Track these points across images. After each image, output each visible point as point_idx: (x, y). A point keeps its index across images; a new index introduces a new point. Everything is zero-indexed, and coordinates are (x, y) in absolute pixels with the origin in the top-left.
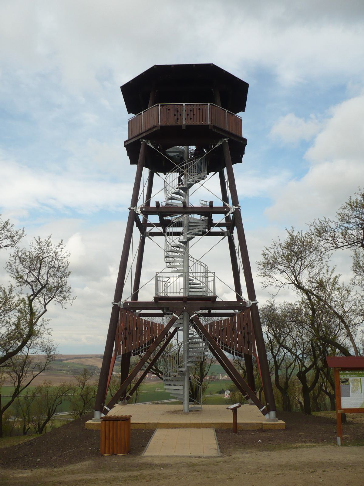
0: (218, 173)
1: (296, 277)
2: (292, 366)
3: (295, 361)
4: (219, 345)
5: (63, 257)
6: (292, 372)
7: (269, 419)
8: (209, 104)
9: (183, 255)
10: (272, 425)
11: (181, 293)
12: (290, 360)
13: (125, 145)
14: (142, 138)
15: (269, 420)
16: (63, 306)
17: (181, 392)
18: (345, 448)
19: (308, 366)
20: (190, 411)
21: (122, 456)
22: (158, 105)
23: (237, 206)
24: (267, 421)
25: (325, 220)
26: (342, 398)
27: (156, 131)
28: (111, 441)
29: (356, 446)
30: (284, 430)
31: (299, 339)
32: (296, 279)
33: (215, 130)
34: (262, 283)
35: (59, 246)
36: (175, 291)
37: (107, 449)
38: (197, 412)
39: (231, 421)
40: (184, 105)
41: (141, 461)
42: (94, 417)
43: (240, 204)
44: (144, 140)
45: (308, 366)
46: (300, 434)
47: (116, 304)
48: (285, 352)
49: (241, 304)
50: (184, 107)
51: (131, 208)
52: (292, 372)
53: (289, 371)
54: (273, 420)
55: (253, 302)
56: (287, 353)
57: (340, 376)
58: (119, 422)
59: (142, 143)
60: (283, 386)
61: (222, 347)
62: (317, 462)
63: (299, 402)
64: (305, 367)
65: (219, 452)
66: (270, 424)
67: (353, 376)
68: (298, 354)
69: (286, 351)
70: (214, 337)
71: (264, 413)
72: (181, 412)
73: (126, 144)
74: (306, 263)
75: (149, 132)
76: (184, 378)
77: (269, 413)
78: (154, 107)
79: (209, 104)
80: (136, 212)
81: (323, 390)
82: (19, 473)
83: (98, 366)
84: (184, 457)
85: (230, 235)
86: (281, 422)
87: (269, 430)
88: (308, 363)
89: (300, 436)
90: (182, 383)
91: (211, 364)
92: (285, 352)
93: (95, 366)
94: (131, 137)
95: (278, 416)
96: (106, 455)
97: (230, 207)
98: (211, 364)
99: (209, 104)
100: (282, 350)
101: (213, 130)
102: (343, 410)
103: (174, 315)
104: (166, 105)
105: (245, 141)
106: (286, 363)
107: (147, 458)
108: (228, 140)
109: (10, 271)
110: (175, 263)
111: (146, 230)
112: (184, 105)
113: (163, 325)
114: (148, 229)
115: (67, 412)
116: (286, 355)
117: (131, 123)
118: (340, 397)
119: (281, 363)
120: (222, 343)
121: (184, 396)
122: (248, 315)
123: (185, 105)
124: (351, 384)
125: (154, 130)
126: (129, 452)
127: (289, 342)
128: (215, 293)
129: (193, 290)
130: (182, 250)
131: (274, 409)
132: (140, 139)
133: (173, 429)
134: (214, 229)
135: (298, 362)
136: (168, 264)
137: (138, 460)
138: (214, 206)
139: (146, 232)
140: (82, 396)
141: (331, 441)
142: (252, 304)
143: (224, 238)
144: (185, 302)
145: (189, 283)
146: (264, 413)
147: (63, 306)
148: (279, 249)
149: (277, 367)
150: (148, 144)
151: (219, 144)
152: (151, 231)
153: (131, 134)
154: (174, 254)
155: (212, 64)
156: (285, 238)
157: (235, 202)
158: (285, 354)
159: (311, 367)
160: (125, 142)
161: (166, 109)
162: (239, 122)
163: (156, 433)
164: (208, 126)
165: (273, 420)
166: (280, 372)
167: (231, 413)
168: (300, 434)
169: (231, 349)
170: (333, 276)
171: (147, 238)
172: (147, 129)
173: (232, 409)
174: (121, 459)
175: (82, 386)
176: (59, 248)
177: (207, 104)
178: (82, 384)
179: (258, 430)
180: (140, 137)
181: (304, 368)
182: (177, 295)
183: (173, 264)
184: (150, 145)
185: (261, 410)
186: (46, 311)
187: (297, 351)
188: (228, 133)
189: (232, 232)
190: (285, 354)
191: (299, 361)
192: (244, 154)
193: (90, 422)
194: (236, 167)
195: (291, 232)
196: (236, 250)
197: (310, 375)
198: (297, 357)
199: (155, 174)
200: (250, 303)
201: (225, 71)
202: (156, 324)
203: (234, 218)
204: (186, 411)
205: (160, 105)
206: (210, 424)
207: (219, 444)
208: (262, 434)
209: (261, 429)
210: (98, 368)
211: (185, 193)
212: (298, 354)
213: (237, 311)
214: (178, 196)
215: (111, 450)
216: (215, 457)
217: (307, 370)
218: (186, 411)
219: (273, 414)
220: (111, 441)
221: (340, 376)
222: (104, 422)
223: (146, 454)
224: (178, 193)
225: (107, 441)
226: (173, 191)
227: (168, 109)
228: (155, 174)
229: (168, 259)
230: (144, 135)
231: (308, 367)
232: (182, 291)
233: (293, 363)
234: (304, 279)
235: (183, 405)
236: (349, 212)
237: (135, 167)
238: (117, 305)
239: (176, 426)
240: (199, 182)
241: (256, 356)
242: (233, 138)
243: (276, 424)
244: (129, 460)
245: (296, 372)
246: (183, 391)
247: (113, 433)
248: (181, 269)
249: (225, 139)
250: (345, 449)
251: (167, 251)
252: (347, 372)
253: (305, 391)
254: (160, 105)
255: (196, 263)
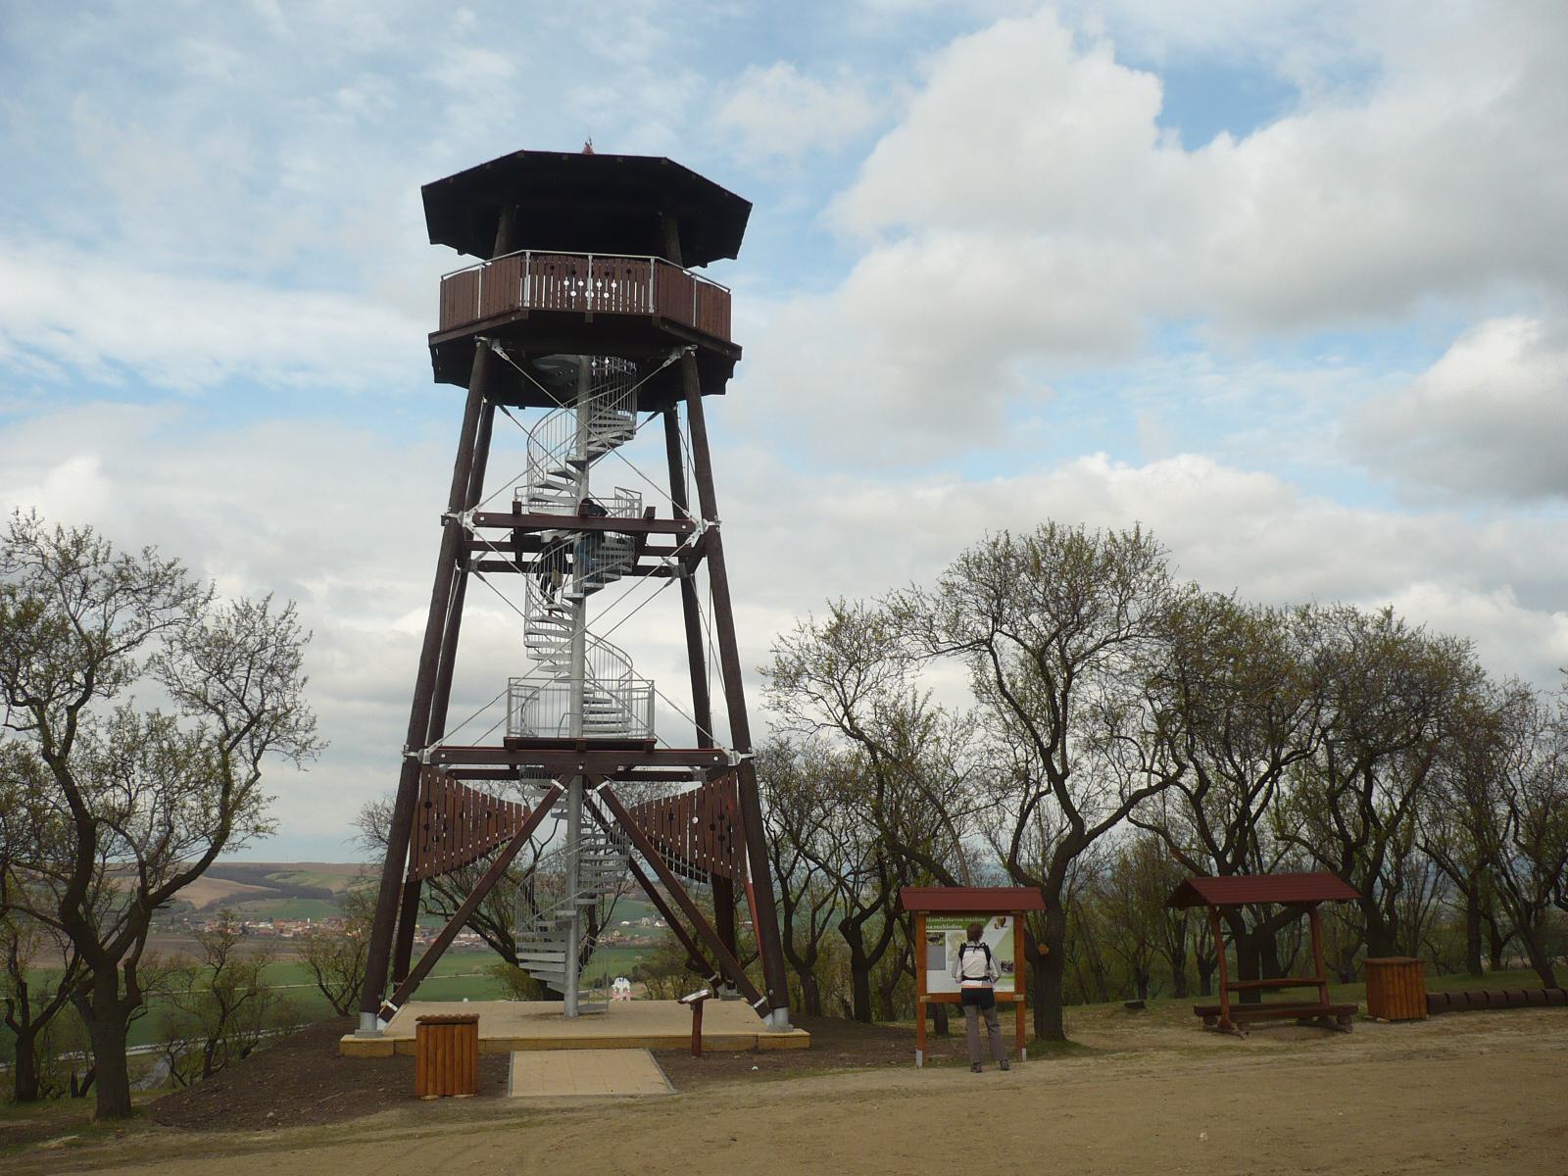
0: (661, 415)
1: (846, 708)
2: (828, 906)
3: (835, 890)
4: (664, 859)
5: (293, 642)
6: (826, 921)
7: (776, 1025)
8: (652, 261)
9: (570, 629)
10: (779, 1040)
11: (564, 729)
12: (823, 888)
13: (433, 343)
14: (480, 334)
15: (771, 1028)
16: (299, 765)
17: (560, 968)
18: (930, 1070)
19: (867, 906)
20: (580, 1014)
21: (466, 1098)
22: (525, 253)
23: (713, 520)
24: (767, 1031)
25: (912, 589)
26: (928, 972)
27: (519, 321)
28: (439, 1068)
29: (617, 573)
30: (805, 1049)
31: (849, 834)
32: (847, 713)
33: (667, 327)
34: (771, 724)
35: (284, 618)
36: (549, 725)
37: (430, 1085)
38: (598, 1016)
39: (688, 1031)
40: (590, 258)
41: (510, 1106)
42: (359, 1028)
43: (721, 515)
44: (483, 338)
45: (867, 906)
46: (842, 1055)
47: (412, 754)
48: (812, 868)
49: (716, 758)
50: (590, 264)
51: (451, 515)
52: (826, 921)
53: (821, 916)
54: (783, 1029)
55: (744, 756)
56: (815, 869)
57: (927, 927)
58: (458, 1027)
59: (478, 344)
60: (803, 957)
61: (671, 863)
62: (871, 1091)
63: (844, 1001)
64: (860, 906)
65: (671, 1087)
66: (775, 1037)
67: (953, 927)
68: (843, 873)
69: (812, 865)
70: (650, 838)
71: (763, 1012)
72: (558, 1017)
73: (436, 340)
74: (869, 681)
75: (500, 322)
76: (568, 934)
77: (773, 1014)
78: (514, 258)
79: (652, 261)
80: (460, 526)
81: (906, 968)
82: (249, 1136)
83: (193, 901)
84: (599, 1096)
85: (686, 576)
86: (800, 1032)
87: (773, 1051)
88: (868, 894)
89: (841, 1059)
90: (561, 946)
91: (616, 899)
92: (812, 868)
93: (183, 900)
94: (447, 327)
95: (794, 1021)
96: (428, 1097)
97: (695, 522)
98: (616, 899)
99: (653, 259)
100: (803, 864)
101: (661, 328)
102: (930, 997)
103: (555, 782)
104: (545, 254)
105: (736, 352)
106: (813, 896)
107: (522, 1101)
108: (696, 351)
109: (162, 677)
110: (548, 652)
111: (469, 555)
112: (590, 258)
113: (527, 808)
114: (475, 555)
115: (143, 1047)
116: (812, 875)
117: (453, 289)
118: (924, 968)
119: (800, 896)
120: (684, 861)
121: (566, 978)
122: (731, 785)
123: (594, 257)
124: (947, 944)
125: (513, 318)
126: (476, 1092)
127: (822, 844)
128: (652, 733)
129: (592, 717)
130: (567, 617)
131: (785, 1004)
132: (474, 334)
133: (551, 1051)
134: (644, 561)
135: (843, 894)
136: (532, 651)
137: (500, 1104)
138: (657, 517)
139: (471, 560)
140: (216, 990)
141: (907, 1061)
142: (742, 759)
143: (671, 582)
144: (581, 752)
145: (584, 701)
146: (763, 1012)
147: (299, 765)
148: (811, 640)
149: (790, 908)
150: (493, 349)
151: (674, 357)
152: (483, 559)
153: (447, 317)
154: (544, 628)
155: (666, 158)
156: (824, 621)
157: (709, 509)
158: (811, 872)
159: (874, 908)
160: (431, 336)
161: (545, 265)
162: (719, 301)
163: (515, 1059)
164: (649, 317)
165: (783, 1029)
166: (795, 920)
167: (688, 1012)
168: (842, 1055)
169: (673, 860)
170: (925, 712)
171: (471, 576)
172: (493, 312)
173: (691, 1003)
174: (461, 1102)
175: (216, 960)
176: (285, 621)
177: (649, 260)
178: (217, 957)
179: (747, 1050)
180: (472, 330)
181: (857, 911)
182: (552, 735)
183: (543, 651)
184: (499, 351)
185: (756, 1005)
186: (258, 775)
187: (841, 865)
188: (695, 332)
189: (692, 568)
190: (811, 872)
191: (845, 891)
192: (731, 377)
193: (346, 1038)
194: (709, 402)
195: (838, 609)
196: (700, 614)
197: (872, 929)
198: (841, 882)
199: (497, 407)
200: (736, 758)
201: (697, 175)
202: (510, 804)
203: (702, 544)
204: (571, 1014)
205: (528, 252)
206: (638, 1038)
207: (667, 1076)
208: (756, 1058)
209: (755, 1048)
210: (194, 908)
211: (579, 472)
212: (843, 873)
213: (698, 768)
214: (562, 480)
215: (439, 1088)
216: (663, 1095)
217: (866, 914)
218: (571, 1014)
219: (781, 1014)
220: (439, 1068)
221: (927, 927)
222: (424, 1028)
223: (514, 1094)
224: (564, 474)
225: (431, 1069)
226: (554, 467)
227: (549, 266)
228: (497, 407)
229: (533, 638)
230: (485, 326)
231: (867, 908)
232: (566, 722)
233: (830, 895)
234: (864, 711)
235: (562, 1002)
236: (960, 579)
237: (457, 397)
238: (416, 758)
239: (559, 1045)
240: (616, 449)
241: (748, 881)
242: (707, 345)
243: (788, 1037)
244: (485, 1105)
245: (838, 918)
246: (563, 965)
247: (444, 1056)
248: (562, 663)
249: (689, 348)
250: (931, 1071)
251: (528, 620)
252: (941, 919)
253: (860, 965)
254: (528, 255)
255: (595, 645)
